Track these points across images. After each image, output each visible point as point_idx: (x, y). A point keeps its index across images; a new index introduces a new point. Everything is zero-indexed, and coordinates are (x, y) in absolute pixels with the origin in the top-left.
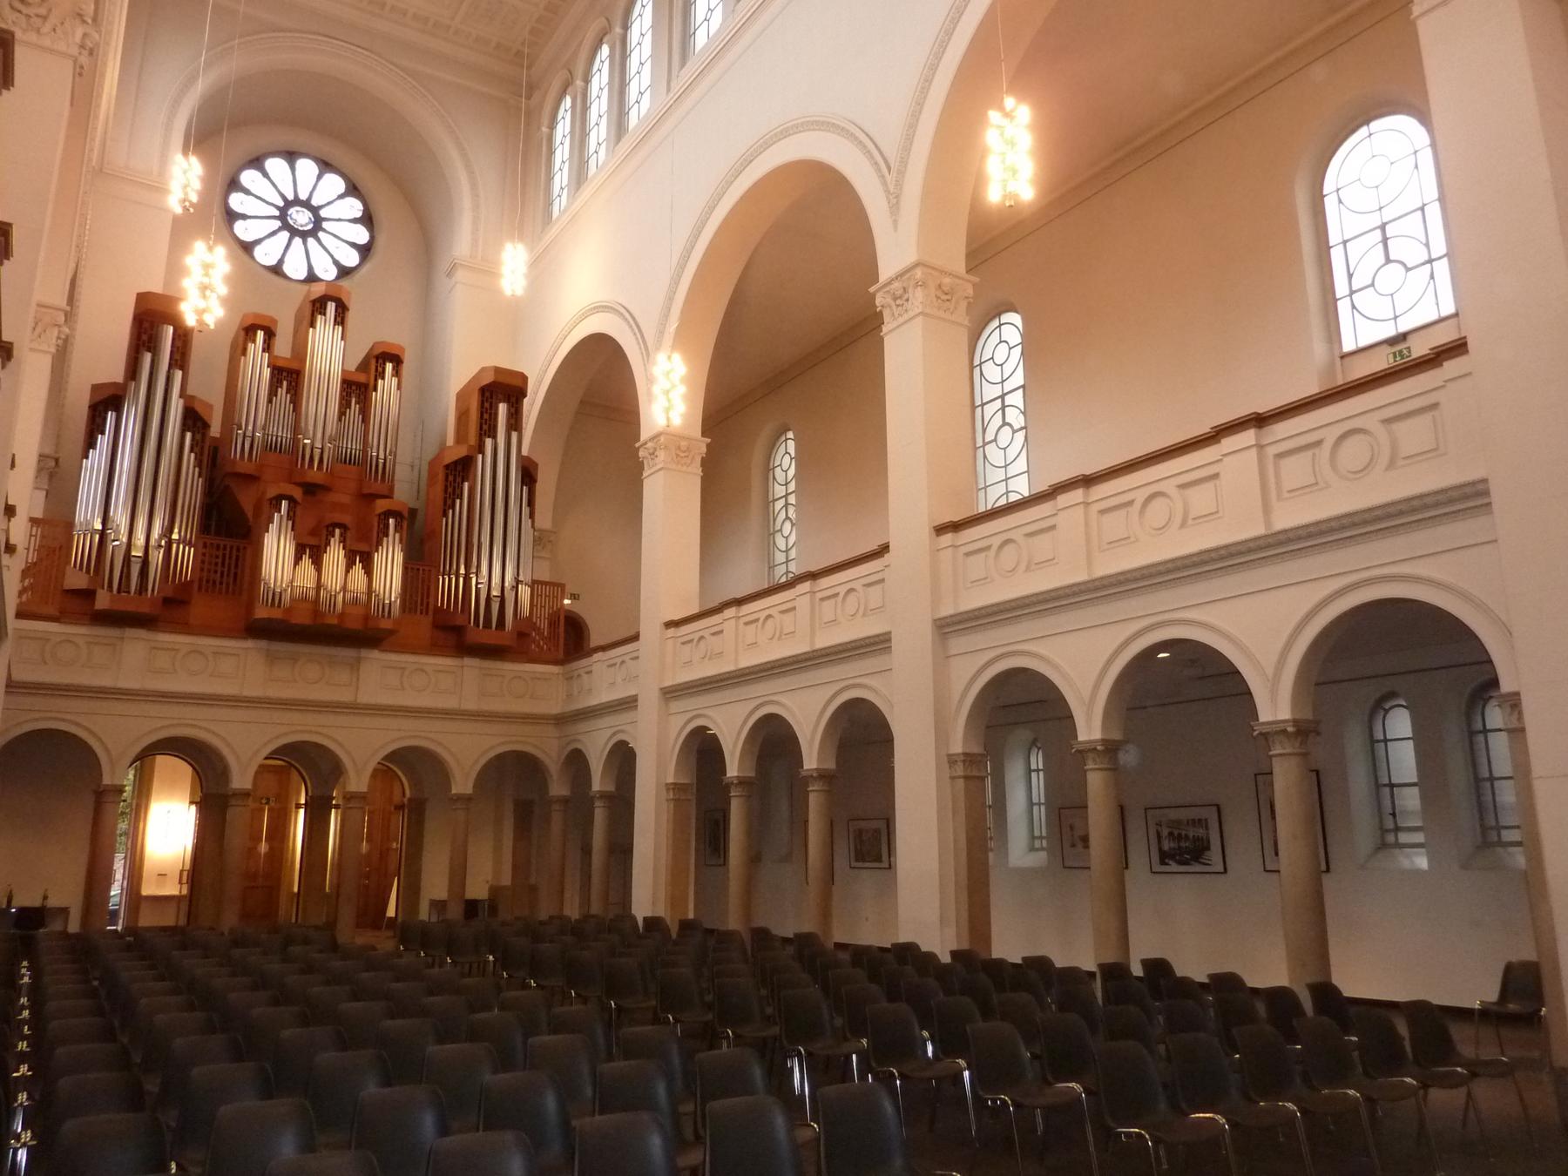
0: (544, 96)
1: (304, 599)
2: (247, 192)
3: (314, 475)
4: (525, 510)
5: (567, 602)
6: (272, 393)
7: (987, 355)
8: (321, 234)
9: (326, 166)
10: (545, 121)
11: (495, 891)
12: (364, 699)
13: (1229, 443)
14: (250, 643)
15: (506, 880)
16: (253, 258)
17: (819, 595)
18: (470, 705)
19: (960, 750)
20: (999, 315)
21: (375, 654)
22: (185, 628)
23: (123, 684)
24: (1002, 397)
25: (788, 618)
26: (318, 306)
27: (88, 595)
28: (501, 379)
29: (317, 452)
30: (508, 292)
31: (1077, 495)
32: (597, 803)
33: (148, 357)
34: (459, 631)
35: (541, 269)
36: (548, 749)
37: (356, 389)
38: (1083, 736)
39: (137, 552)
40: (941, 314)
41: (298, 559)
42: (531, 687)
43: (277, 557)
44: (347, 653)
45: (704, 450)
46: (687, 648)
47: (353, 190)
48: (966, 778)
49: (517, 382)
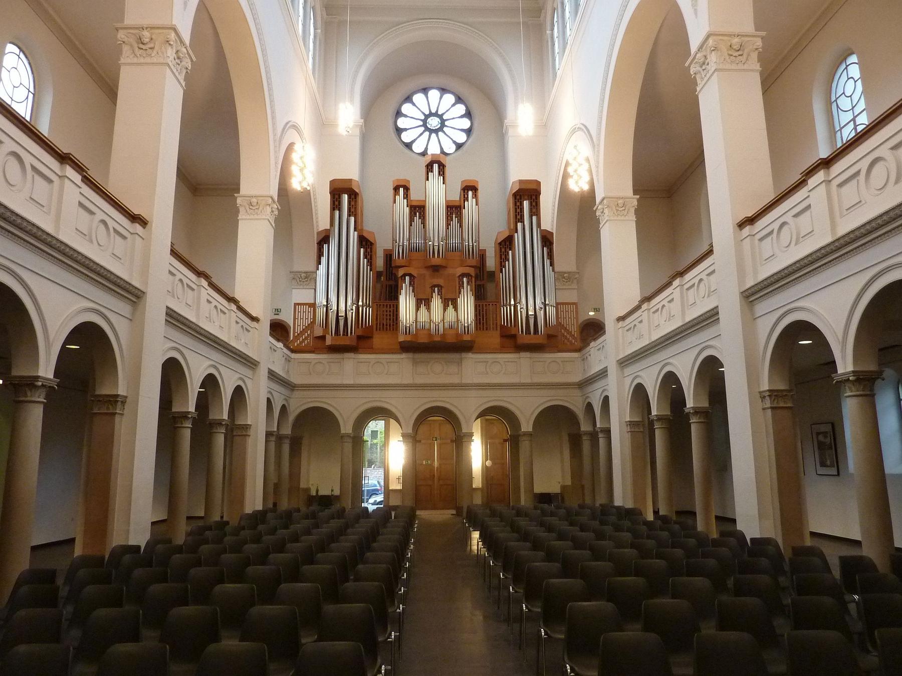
0: (545, 17)
1: (423, 328)
3: (436, 261)
4: (547, 262)
5: (591, 313)
6: (411, 220)
7: (840, 92)
8: (445, 129)
9: (443, 91)
10: (549, 27)
11: (564, 487)
12: (465, 381)
13: (813, 181)
14: (404, 356)
15: (568, 482)
16: (411, 150)
17: (686, 287)
18: (528, 381)
19: (766, 388)
20: (845, 59)
21: (470, 355)
22: (371, 350)
24: (854, 120)
25: (671, 305)
26: (429, 167)
27: (323, 338)
28: (524, 187)
29: (436, 248)
31: (820, 176)
32: (693, 420)
33: (337, 213)
34: (514, 337)
36: (575, 404)
37: (454, 210)
38: (840, 370)
39: (342, 314)
40: (734, 67)
41: (418, 308)
42: (557, 367)
43: (406, 305)
44: (455, 356)
45: (636, 203)
46: (692, 291)
47: (459, 100)
48: (772, 408)
49: (534, 187)
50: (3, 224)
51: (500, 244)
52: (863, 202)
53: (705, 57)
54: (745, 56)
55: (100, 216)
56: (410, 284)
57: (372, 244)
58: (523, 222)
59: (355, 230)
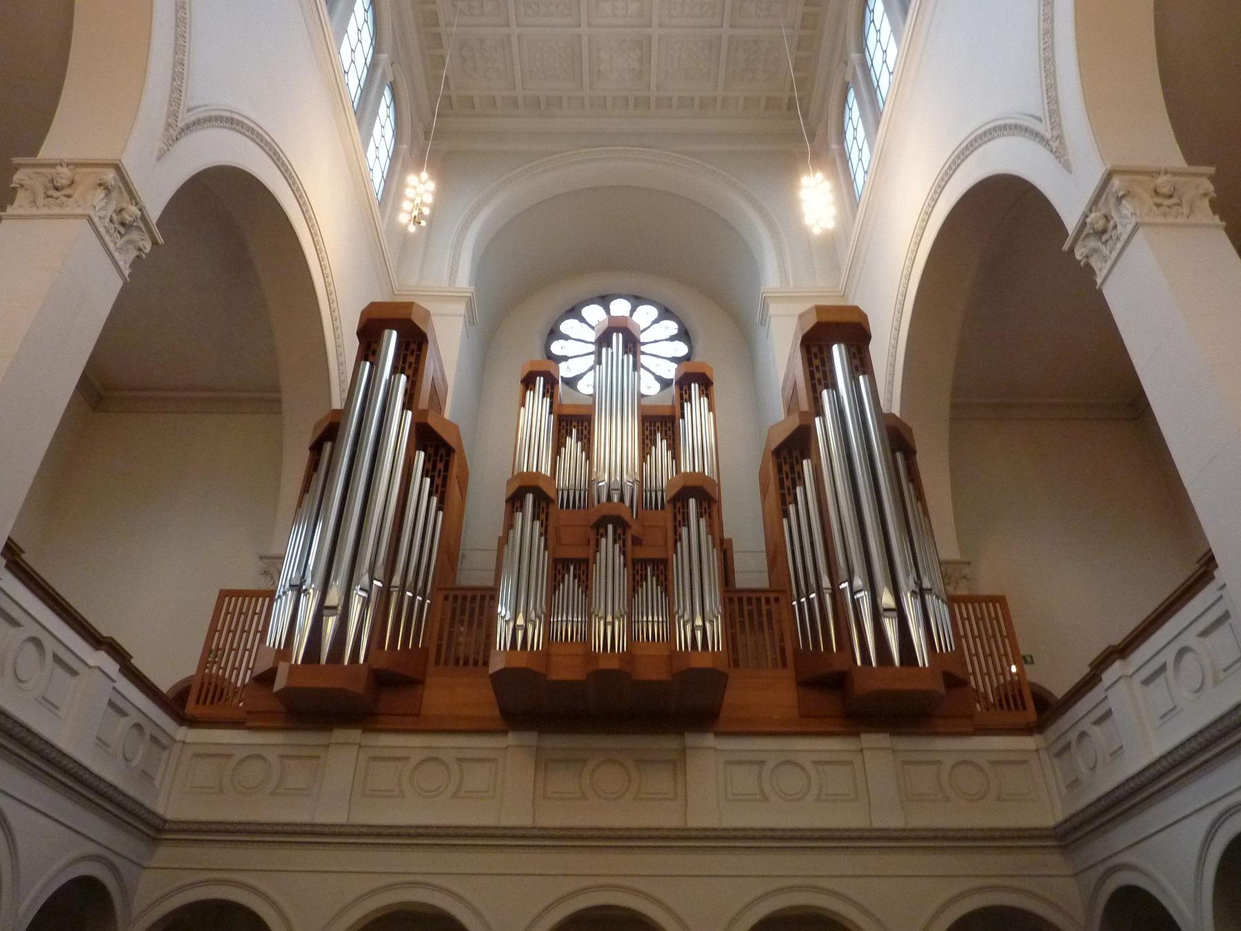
2: (567, 338)
13: (1109, 676)
14: (512, 739)
18: (893, 820)
21: (709, 740)
22: (417, 723)
23: (324, 817)
30: (816, 231)
35: (848, 197)
44: (668, 743)
47: (666, 313)
50: (5, 743)
51: (777, 453)
52: (1179, 708)
53: (1107, 218)
54: (1185, 210)
55: (31, 630)
56: (535, 516)
57: (450, 450)
58: (834, 386)
59: (407, 405)
